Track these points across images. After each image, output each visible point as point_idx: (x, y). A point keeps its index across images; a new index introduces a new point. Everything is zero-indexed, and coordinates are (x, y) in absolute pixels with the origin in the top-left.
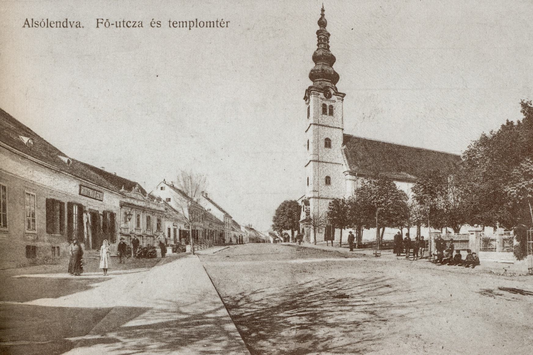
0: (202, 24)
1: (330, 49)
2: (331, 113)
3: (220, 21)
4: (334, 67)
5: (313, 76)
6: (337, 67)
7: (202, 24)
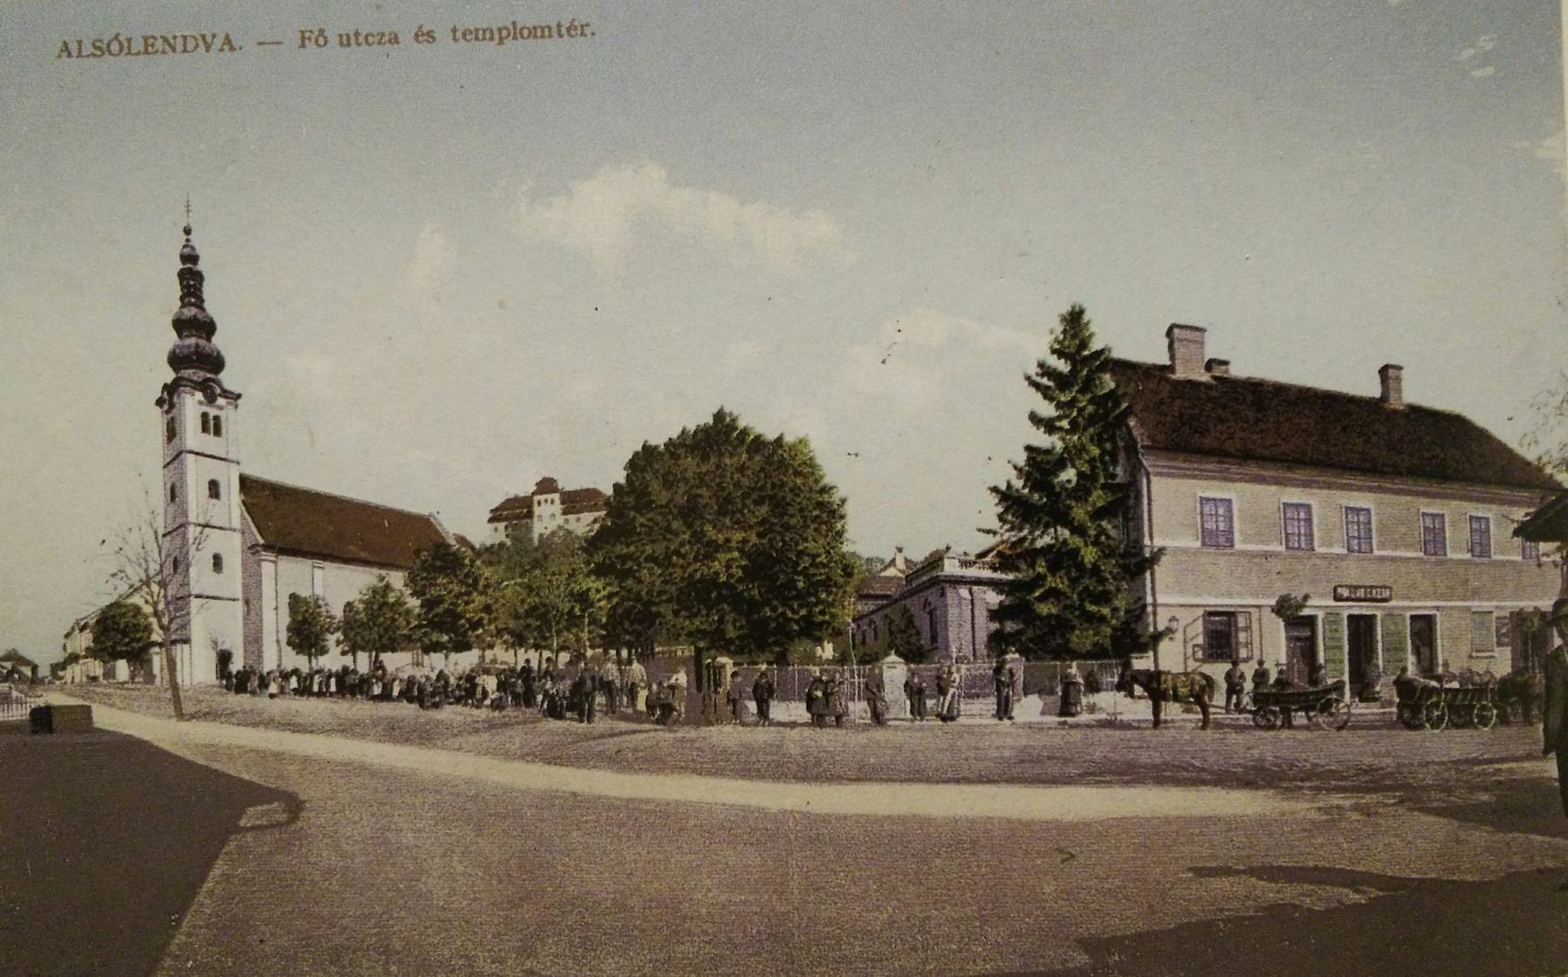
0: (525, 33)
1: (206, 305)
2: (217, 432)
3: (566, 24)
4: (214, 339)
5: (176, 360)
6: (217, 340)
7: (525, 33)
